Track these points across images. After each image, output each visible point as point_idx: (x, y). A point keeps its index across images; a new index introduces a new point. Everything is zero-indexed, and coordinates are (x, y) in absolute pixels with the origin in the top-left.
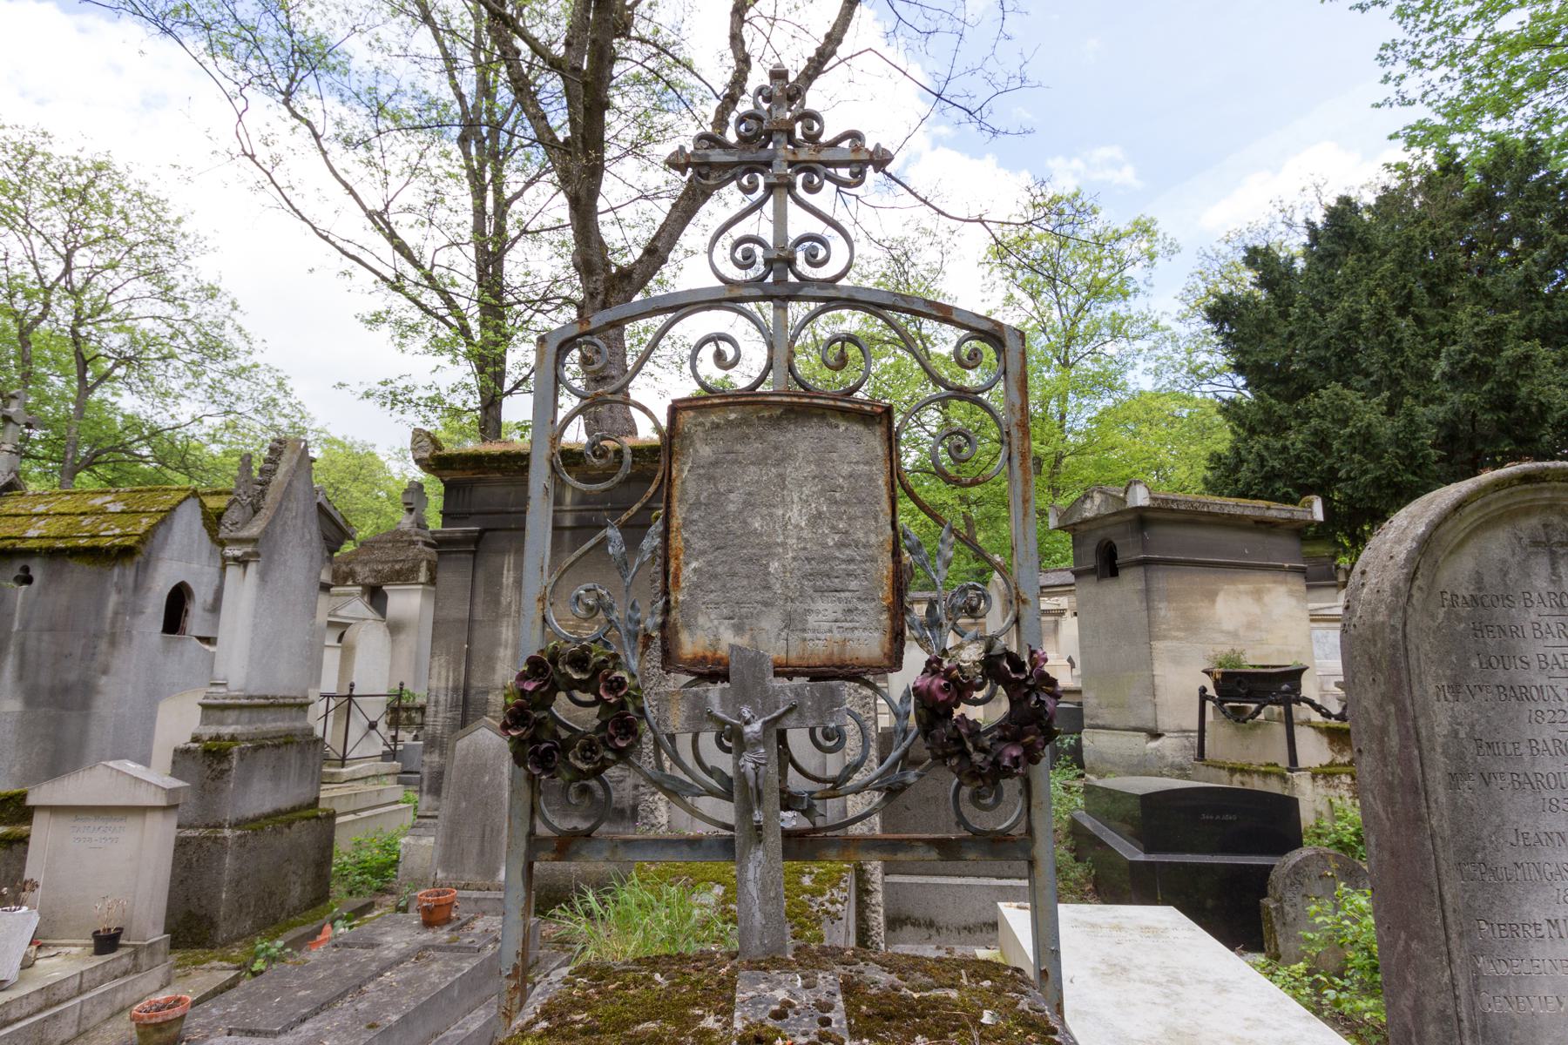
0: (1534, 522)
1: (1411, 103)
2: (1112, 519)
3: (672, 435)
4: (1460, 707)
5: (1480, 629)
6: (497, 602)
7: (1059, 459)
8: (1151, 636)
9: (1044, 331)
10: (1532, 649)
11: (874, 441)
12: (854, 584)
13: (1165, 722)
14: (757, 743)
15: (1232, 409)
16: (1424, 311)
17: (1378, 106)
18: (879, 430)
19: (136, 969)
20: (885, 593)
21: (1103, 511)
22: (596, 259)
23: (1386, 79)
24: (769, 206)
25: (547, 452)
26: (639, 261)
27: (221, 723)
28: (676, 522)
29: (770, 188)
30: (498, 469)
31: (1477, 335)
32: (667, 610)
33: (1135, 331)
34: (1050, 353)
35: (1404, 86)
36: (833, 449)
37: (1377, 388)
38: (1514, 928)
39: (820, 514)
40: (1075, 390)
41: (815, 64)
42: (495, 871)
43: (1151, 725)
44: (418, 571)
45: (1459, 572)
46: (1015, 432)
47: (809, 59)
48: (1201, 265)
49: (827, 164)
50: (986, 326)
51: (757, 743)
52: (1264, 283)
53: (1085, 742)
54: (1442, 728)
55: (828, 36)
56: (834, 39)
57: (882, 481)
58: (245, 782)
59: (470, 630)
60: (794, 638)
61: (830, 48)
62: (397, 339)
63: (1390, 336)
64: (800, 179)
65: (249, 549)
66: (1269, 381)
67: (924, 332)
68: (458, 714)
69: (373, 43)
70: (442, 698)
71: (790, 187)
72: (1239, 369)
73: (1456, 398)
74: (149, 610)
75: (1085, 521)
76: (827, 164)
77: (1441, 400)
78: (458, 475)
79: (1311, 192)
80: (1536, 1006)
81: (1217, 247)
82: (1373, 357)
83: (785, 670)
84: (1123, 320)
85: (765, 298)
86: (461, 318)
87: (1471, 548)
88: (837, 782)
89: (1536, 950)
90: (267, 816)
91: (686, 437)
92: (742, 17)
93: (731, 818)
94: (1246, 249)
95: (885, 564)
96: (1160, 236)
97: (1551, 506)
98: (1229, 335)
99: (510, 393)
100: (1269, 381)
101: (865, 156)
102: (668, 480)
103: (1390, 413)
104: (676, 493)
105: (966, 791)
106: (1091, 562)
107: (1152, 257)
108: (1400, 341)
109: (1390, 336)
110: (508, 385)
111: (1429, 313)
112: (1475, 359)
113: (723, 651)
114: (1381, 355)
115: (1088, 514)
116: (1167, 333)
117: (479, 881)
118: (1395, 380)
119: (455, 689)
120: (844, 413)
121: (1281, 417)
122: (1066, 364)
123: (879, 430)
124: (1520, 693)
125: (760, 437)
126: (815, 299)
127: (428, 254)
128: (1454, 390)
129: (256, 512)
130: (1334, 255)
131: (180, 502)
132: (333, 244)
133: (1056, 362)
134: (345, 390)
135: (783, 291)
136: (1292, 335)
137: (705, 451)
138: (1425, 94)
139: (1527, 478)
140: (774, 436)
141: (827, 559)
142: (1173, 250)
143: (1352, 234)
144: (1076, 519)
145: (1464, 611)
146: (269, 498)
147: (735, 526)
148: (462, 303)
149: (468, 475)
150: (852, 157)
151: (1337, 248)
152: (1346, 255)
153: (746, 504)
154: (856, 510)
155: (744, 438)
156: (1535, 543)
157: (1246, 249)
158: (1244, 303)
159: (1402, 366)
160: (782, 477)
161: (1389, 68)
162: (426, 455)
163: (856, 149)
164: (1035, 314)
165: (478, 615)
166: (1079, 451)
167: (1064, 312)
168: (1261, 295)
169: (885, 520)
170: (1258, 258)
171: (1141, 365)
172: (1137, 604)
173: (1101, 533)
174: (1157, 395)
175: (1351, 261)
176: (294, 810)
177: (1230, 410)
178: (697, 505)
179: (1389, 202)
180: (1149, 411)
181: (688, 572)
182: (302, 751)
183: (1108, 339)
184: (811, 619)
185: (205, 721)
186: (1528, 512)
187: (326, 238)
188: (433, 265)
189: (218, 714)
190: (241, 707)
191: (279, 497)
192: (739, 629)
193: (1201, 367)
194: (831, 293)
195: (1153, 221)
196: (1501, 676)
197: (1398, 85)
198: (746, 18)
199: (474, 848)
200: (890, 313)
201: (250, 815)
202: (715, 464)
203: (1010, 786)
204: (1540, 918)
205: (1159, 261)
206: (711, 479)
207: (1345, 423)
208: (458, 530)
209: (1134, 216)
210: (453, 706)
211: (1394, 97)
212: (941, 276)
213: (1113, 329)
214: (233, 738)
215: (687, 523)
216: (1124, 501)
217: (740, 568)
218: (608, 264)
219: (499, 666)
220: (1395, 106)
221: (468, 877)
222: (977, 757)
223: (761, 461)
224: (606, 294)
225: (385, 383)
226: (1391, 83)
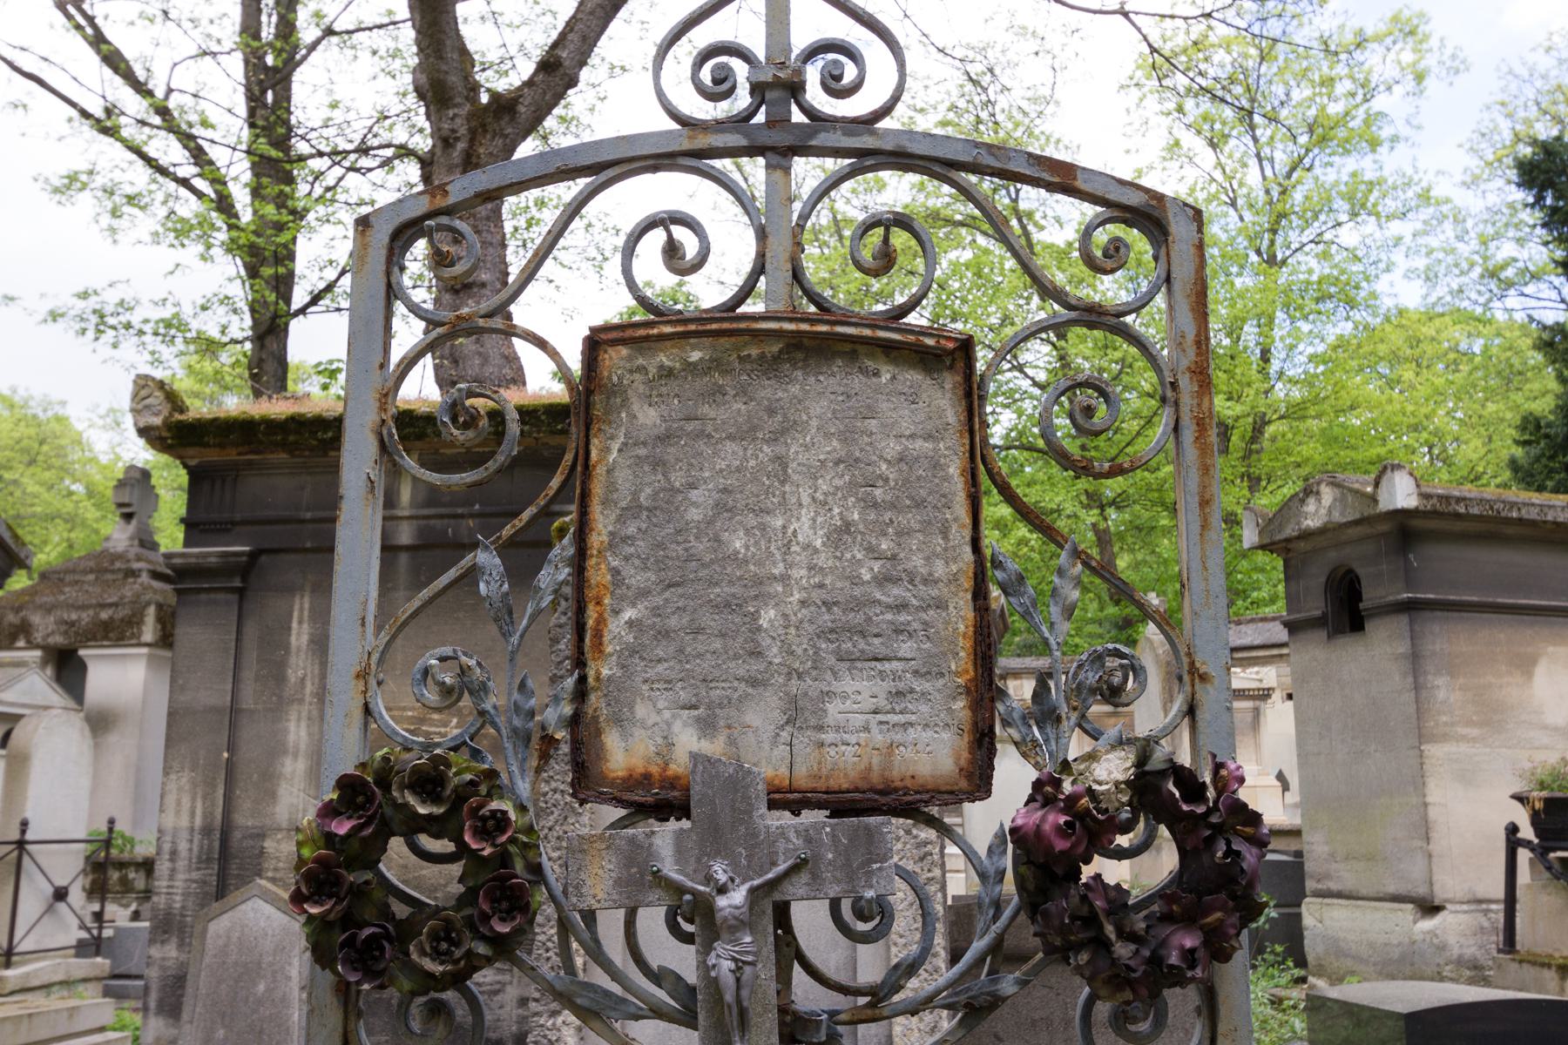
6: (280, 678)
8: (1422, 736)
12: (906, 648)
13: (1447, 885)
18: (950, 380)
20: (961, 662)
21: (1337, 517)
25: (372, 417)
28: (597, 540)
30: (284, 446)
32: (581, 693)
33: (1391, 205)
36: (870, 413)
39: (847, 527)
43: (1422, 890)
44: (140, 622)
48: (1503, 90)
51: (740, 924)
53: (1308, 920)
59: (233, 726)
60: (803, 741)
62: (106, 220)
70: (183, 846)
75: (1306, 535)
78: (213, 456)
83: (786, 798)
84: (1371, 185)
85: (752, 151)
86: (218, 181)
95: (962, 612)
96: (1434, 42)
99: (302, 311)
102: (584, 466)
104: (598, 488)
105: (1103, 1009)
106: (1315, 606)
107: (1419, 78)
113: (680, 764)
115: (1311, 523)
119: (207, 831)
120: (889, 350)
123: (950, 380)
125: (743, 392)
126: (836, 153)
133: (1254, 258)
135: (779, 138)
137: (648, 417)
140: (768, 390)
141: (858, 604)
142: (1457, 67)
144: (1290, 531)
147: (700, 547)
148: (218, 155)
149: (231, 455)
153: (720, 507)
154: (911, 519)
155: (715, 394)
162: (157, 421)
164: (1218, 175)
165: (248, 700)
166: (1295, 412)
167: (1269, 172)
172: (1396, 679)
173: (1333, 556)
178: (634, 510)
180: (1415, 342)
181: (618, 629)
183: (1344, 217)
184: (833, 710)
192: (707, 726)
193: (1503, 267)
194: (866, 142)
202: (665, 438)
206: (658, 464)
210: (204, 860)
212: (1051, 108)
215: (617, 541)
216: (1373, 499)
217: (709, 620)
222: (1123, 950)
223: (746, 434)
224: (472, 141)
225: (84, 295)
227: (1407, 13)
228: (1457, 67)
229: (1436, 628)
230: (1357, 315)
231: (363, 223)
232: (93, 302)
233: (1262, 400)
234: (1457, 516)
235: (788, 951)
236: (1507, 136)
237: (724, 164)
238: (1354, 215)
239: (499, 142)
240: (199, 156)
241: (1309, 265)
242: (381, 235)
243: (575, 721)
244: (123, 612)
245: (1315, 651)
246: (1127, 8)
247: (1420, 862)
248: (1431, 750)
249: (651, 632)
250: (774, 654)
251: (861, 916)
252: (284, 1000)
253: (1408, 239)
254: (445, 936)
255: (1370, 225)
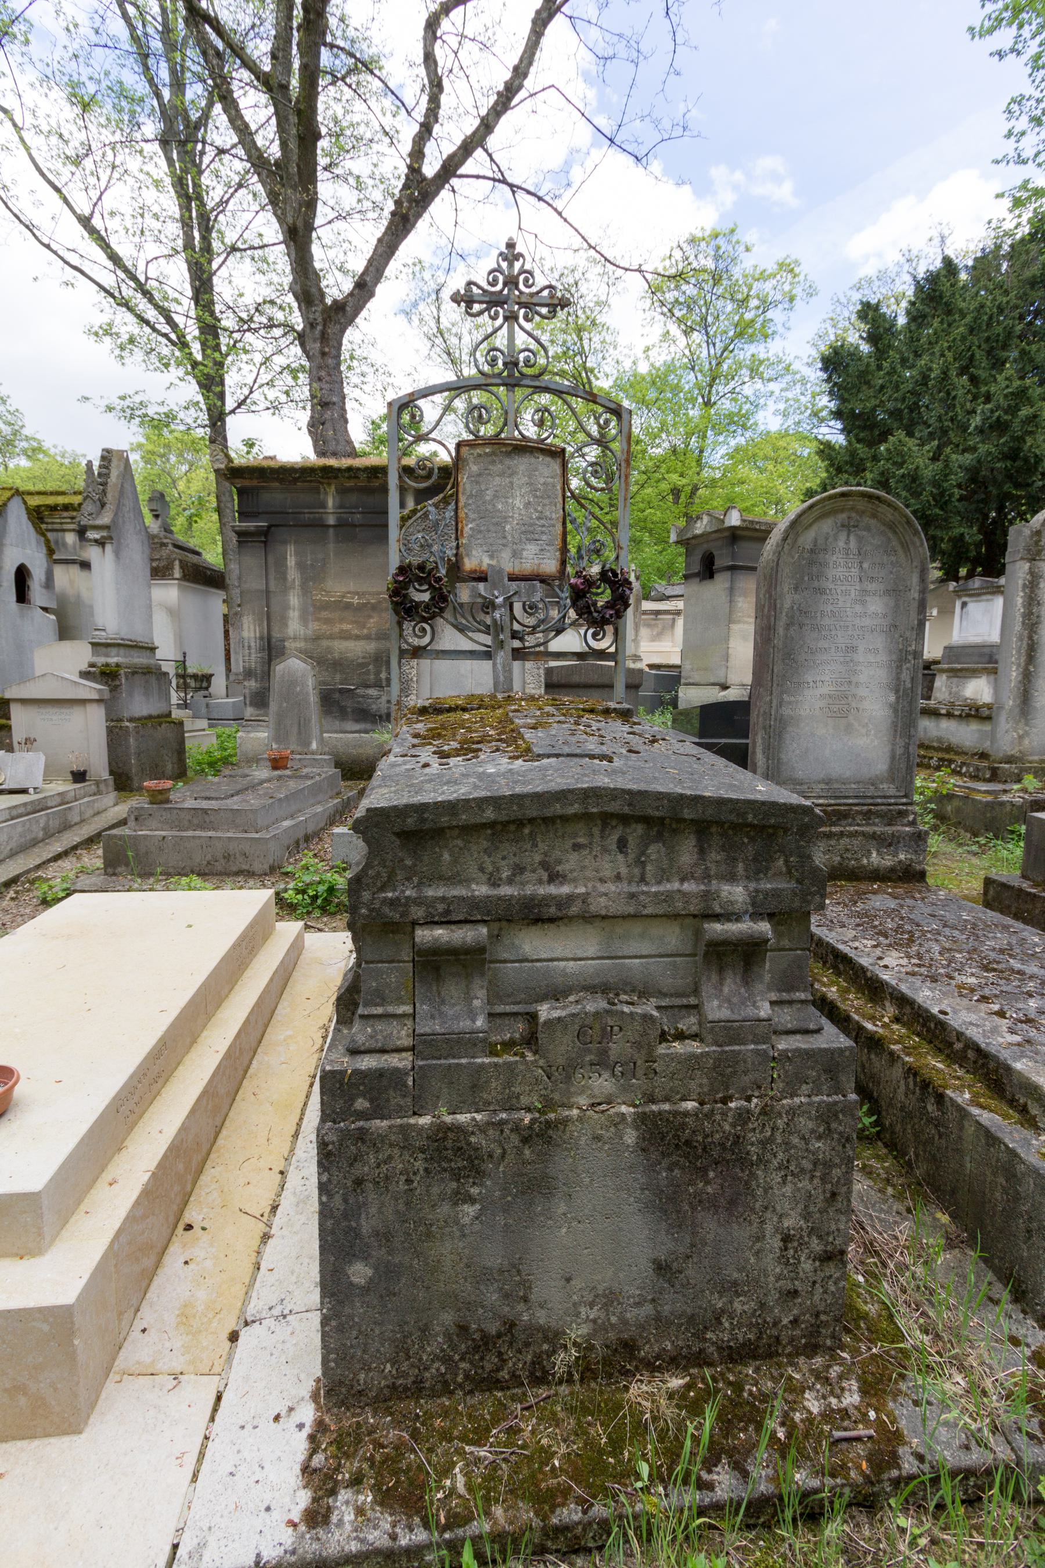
0: (844, 516)
1: (1024, 162)
2: (714, 536)
3: (458, 459)
4: (797, 596)
5: (811, 563)
6: (285, 579)
7: (695, 489)
8: (730, 621)
9: (693, 369)
10: (831, 573)
11: (555, 466)
12: (544, 537)
13: (733, 678)
14: (501, 606)
15: (827, 451)
16: (980, 372)
17: (997, 162)
18: (559, 461)
19: (99, 792)
20: (558, 542)
21: (709, 529)
22: (314, 290)
23: (1009, 134)
24: (505, 330)
25: (396, 466)
26: (351, 294)
27: (107, 655)
28: (461, 504)
29: (506, 319)
30: (277, 479)
31: (1006, 396)
32: (458, 547)
33: (768, 373)
34: (696, 392)
35: (1025, 141)
36: (536, 470)
37: (931, 436)
38: (799, 684)
39: (529, 503)
40: (713, 428)
41: (504, 99)
42: (309, 744)
43: (723, 681)
44: (172, 568)
45: (807, 539)
46: (623, 464)
47: (498, 93)
48: (833, 311)
49: (536, 305)
50: (613, 406)
51: (501, 606)
52: (872, 338)
53: (680, 694)
54: (787, 603)
55: (516, 69)
56: (520, 72)
57: (559, 487)
58: (130, 694)
59: (268, 598)
60: (517, 561)
61: (517, 82)
62: (117, 352)
63: (948, 393)
64: (522, 311)
65: (105, 534)
66: (859, 427)
67: (588, 365)
68: (265, 655)
69: (71, 27)
70: (253, 644)
71: (516, 318)
72: (838, 414)
73: (983, 448)
74: (5, 584)
75: (695, 537)
76: (536, 305)
77: (974, 449)
78: (247, 483)
79: (937, 241)
80: (802, 713)
81: (849, 293)
82: (933, 412)
83: (512, 578)
84: (761, 362)
85: (503, 385)
86: (181, 336)
87: (815, 527)
88: (534, 628)
89: (806, 692)
90: (146, 718)
91: (465, 460)
92: (434, 33)
93: (489, 643)
94: (862, 303)
95: (559, 528)
96: (802, 277)
97: (852, 509)
98: (835, 384)
99: (233, 411)
100: (859, 427)
101: (556, 302)
102: (456, 485)
103: (935, 459)
104: (461, 489)
105: (591, 631)
106: (696, 568)
107: (792, 299)
108: (954, 398)
109: (948, 393)
110: (230, 404)
111: (983, 374)
112: (999, 417)
113: (484, 567)
114: (938, 409)
115: (698, 532)
116: (798, 376)
117: (299, 749)
118: (944, 432)
119: (261, 638)
120: (542, 450)
121: (862, 460)
122: (708, 404)
123: (559, 461)
124: (821, 591)
125: (501, 462)
126: (528, 386)
127: (141, 267)
128: (983, 442)
129: (103, 505)
130: (924, 316)
131: (9, 499)
132: (55, 253)
133: (700, 400)
134: (88, 404)
135: (512, 381)
136: (882, 387)
137: (474, 468)
138: (1037, 155)
139: (843, 495)
140: (508, 462)
141: (532, 525)
142: (811, 292)
143: (941, 297)
144: (689, 535)
145: (806, 555)
146: (109, 496)
147: (489, 507)
148: (179, 320)
149: (255, 483)
150: (549, 301)
151: (927, 310)
152: (933, 317)
153: (495, 496)
154: (546, 501)
155: (493, 462)
156: (843, 526)
157: (862, 303)
158: (851, 354)
159: (952, 420)
160: (511, 483)
161: (1013, 122)
162: (222, 466)
163: (552, 296)
164: (687, 352)
165: (272, 588)
166: (713, 483)
167: (712, 351)
168: (865, 348)
169: (560, 506)
170: (869, 312)
171: (772, 406)
172: (724, 598)
173: (705, 546)
174: (784, 434)
175: (936, 323)
176: (158, 717)
177: (826, 450)
178: (471, 496)
179: (984, 264)
180: (776, 450)
181: (467, 530)
182: (158, 679)
183: (747, 379)
184: (525, 553)
185: (94, 653)
186: (842, 511)
187: (48, 247)
188: (147, 279)
189: (104, 649)
190: (119, 645)
191: (117, 494)
192: (491, 557)
193: (821, 410)
194: (537, 384)
195: (797, 263)
196: (816, 584)
197: (1018, 141)
198: (439, 34)
199: (295, 730)
200: (569, 398)
201: (137, 715)
202: (480, 475)
203: (609, 629)
204: (810, 680)
205: (798, 303)
206: (477, 483)
207: (901, 465)
208: (251, 525)
209: (780, 256)
210: (262, 649)
211: (1012, 154)
212: (606, 309)
213: (752, 370)
214: (118, 665)
215: (466, 505)
216: (723, 521)
217: (492, 528)
218: (322, 295)
219: (290, 623)
220: (1011, 163)
221: (293, 747)
222: (595, 615)
223: (502, 474)
224: (324, 326)
225: (123, 398)
226: (1013, 139)
227: (788, 261)
228: (811, 292)
229: (968, 743)
230: (748, 434)
231: (390, 404)
232: (128, 402)
233: (696, 477)
234: (756, 530)
235: (513, 618)
236: (832, 338)
237: (494, 389)
238: (752, 378)
239: (338, 326)
240: (170, 321)
241: (726, 405)
242: (396, 408)
243: (456, 555)
244: (163, 564)
245: (695, 587)
246: (643, 268)
247: (724, 670)
248: (733, 627)
249: (476, 531)
250: (509, 538)
251: (531, 608)
252: (307, 693)
253: (777, 393)
254: (427, 607)
255: (759, 385)
